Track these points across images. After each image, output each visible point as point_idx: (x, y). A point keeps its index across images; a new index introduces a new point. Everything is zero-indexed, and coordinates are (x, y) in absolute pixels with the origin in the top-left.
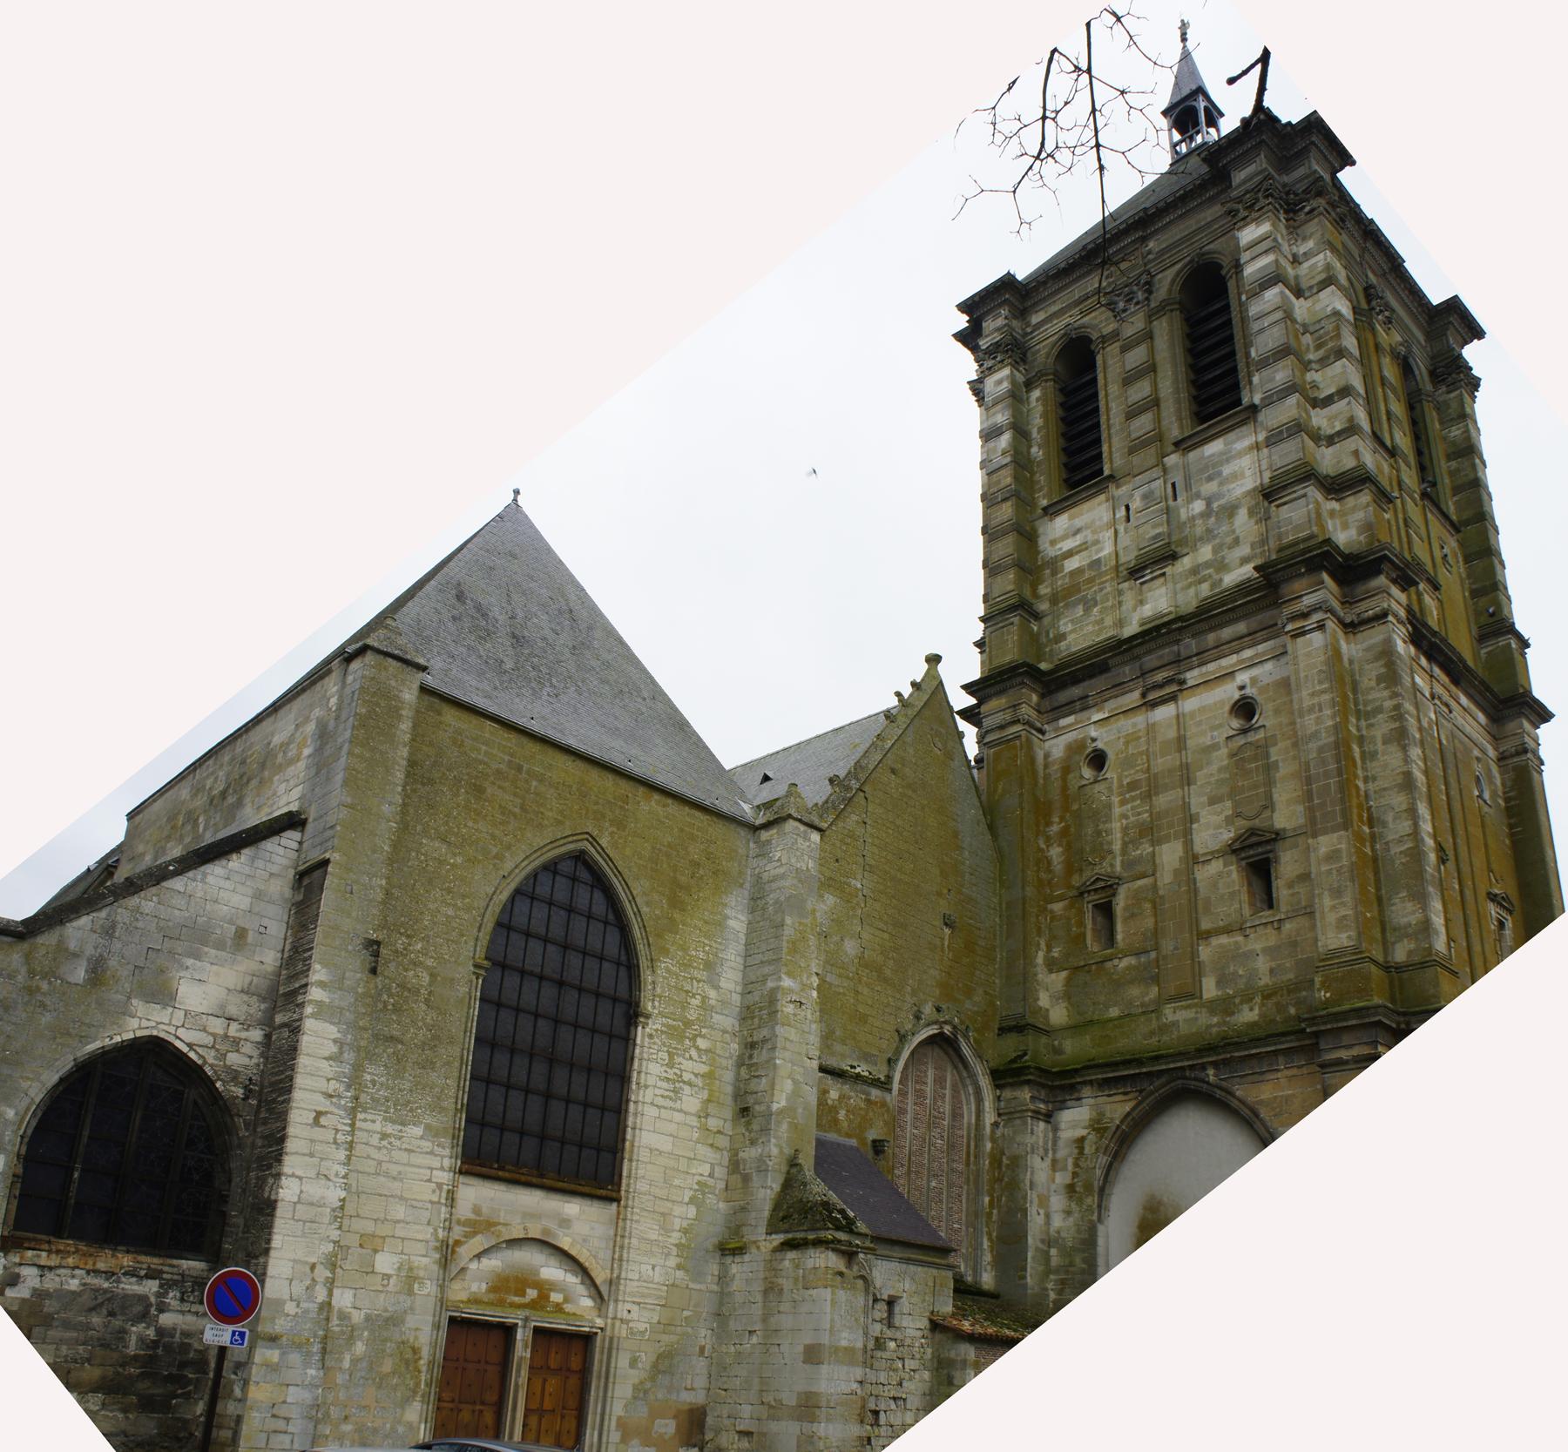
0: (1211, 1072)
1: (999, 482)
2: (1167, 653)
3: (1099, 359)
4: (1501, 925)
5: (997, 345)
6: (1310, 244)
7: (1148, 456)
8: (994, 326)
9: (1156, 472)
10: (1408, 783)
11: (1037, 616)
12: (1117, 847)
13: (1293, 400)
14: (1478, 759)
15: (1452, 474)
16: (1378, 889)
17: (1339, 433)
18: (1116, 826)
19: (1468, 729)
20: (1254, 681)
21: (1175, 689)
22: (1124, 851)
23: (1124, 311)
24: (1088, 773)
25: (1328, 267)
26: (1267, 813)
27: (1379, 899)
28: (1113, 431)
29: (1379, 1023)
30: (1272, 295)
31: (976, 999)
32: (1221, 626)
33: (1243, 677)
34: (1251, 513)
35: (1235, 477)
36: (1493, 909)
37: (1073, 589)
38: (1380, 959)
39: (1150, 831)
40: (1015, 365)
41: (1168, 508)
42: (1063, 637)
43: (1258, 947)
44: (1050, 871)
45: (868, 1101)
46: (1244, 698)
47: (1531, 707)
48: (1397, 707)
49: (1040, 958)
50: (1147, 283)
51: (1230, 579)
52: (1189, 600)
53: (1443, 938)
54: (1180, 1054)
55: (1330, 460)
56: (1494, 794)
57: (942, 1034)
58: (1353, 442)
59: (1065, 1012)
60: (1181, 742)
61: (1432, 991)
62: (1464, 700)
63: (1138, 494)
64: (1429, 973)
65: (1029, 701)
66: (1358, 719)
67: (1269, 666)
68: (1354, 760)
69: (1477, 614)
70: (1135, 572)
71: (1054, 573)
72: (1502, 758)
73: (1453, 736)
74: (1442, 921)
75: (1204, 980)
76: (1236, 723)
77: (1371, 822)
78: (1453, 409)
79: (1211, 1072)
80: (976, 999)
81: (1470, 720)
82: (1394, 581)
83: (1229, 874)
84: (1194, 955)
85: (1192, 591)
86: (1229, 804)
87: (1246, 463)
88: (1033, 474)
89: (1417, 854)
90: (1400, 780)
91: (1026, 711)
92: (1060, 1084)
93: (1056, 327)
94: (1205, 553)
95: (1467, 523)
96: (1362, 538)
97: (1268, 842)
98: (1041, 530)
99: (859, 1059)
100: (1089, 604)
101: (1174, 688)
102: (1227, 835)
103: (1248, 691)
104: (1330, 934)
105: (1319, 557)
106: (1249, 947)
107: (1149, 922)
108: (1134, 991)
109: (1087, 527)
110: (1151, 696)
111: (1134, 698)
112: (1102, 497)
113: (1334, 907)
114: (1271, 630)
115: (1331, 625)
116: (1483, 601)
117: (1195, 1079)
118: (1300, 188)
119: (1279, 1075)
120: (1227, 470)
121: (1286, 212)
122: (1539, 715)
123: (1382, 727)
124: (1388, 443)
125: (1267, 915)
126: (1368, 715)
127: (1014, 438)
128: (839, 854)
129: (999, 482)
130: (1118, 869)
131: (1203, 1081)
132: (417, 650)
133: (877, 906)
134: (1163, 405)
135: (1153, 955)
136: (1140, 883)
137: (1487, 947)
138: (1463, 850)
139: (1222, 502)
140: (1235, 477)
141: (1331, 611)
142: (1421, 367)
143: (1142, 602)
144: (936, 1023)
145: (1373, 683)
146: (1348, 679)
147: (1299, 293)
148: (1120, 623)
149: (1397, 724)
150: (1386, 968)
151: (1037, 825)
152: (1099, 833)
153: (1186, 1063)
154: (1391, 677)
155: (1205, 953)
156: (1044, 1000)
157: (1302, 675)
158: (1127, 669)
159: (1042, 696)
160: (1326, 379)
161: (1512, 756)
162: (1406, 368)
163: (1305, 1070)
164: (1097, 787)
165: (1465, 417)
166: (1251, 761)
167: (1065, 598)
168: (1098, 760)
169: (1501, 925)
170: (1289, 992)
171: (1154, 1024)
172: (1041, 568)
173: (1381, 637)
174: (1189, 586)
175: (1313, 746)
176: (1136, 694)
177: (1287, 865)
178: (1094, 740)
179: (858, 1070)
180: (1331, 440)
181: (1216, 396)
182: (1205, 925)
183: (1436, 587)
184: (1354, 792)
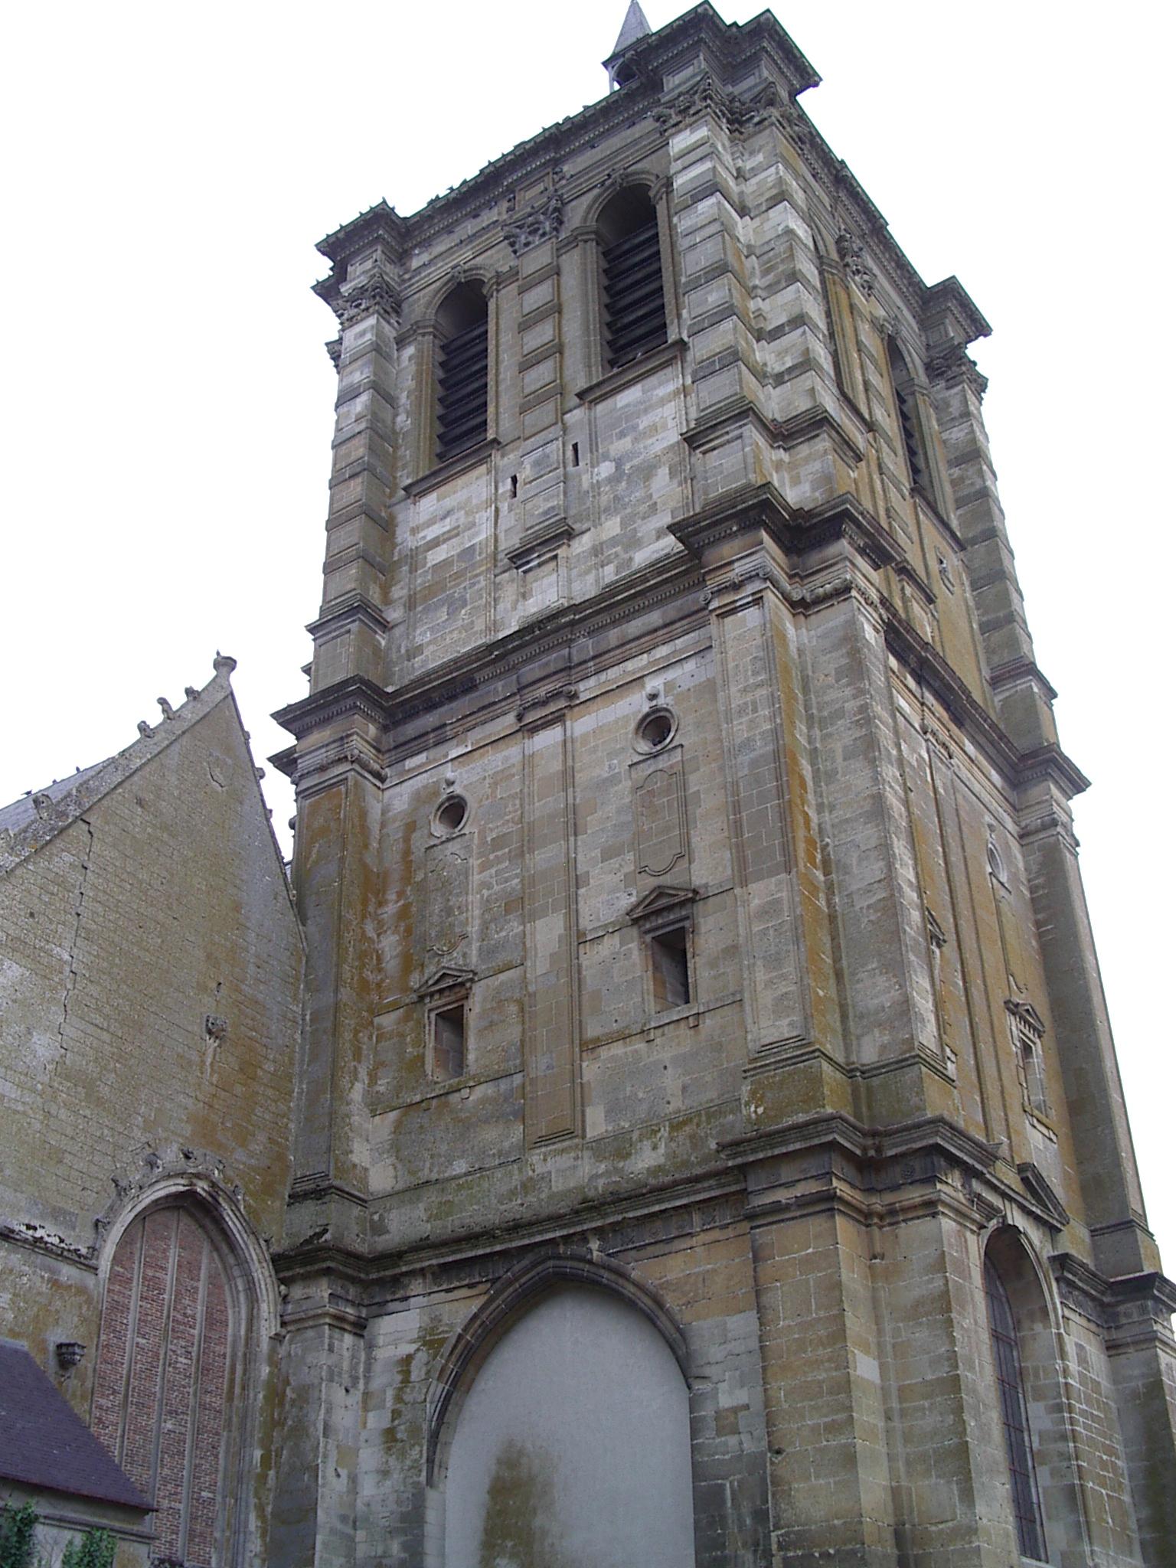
0: (594, 1245)
1: (349, 455)
2: (554, 659)
3: (492, 306)
4: (1027, 1050)
5: (363, 290)
6: (760, 157)
7: (545, 413)
8: (359, 274)
9: (556, 431)
10: (878, 810)
11: (385, 626)
12: (474, 929)
13: (728, 325)
14: (990, 826)
15: (954, 483)
16: (837, 960)
17: (790, 370)
18: (474, 898)
19: (977, 788)
20: (669, 686)
21: (562, 705)
22: (484, 935)
23: (527, 244)
24: (439, 830)
25: (780, 181)
26: (683, 864)
27: (839, 975)
28: (502, 387)
29: (833, 1145)
30: (707, 207)
31: (253, 1147)
32: (627, 617)
33: (654, 684)
34: (672, 474)
35: (654, 429)
36: (1013, 1022)
37: (434, 589)
38: (841, 1060)
39: (519, 904)
40: (385, 314)
41: (565, 475)
42: (419, 649)
43: (666, 1056)
44: (380, 970)
45: (55, 1283)
46: (655, 710)
47: (1060, 769)
48: (864, 708)
49: (357, 1093)
50: (556, 210)
51: (642, 558)
52: (586, 588)
53: (931, 1027)
54: (550, 1218)
55: (775, 403)
56: (1014, 877)
57: (190, 1195)
58: (810, 379)
59: (391, 1172)
60: (568, 776)
61: (915, 1100)
62: (970, 748)
63: (528, 461)
64: (910, 1074)
65: (363, 733)
66: (810, 727)
67: (690, 666)
68: (802, 778)
69: (990, 651)
70: (519, 558)
71: (413, 570)
72: (1023, 836)
73: (955, 791)
74: (930, 1005)
75: (588, 1111)
76: (644, 747)
77: (826, 867)
78: (955, 408)
79: (594, 1245)
80: (253, 1147)
81: (979, 780)
82: (862, 551)
83: (627, 955)
84: (575, 1073)
85: (591, 578)
86: (630, 856)
87: (670, 410)
88: (396, 448)
89: (891, 907)
90: (867, 806)
91: (358, 745)
92: (374, 1278)
93: (440, 271)
94: (612, 527)
95: (974, 541)
96: (817, 494)
97: (682, 904)
98: (400, 517)
99: (42, 1216)
100: (454, 606)
101: (562, 703)
102: (626, 901)
103: (661, 702)
104: (764, 1023)
105: (756, 510)
106: (655, 1057)
107: (514, 1033)
108: (490, 1134)
109: (460, 508)
110: (529, 718)
111: (508, 721)
112: (483, 468)
113: (770, 983)
114: (696, 618)
115: (771, 598)
116: (996, 637)
117: (572, 1258)
118: (747, 97)
119: (694, 1241)
120: (644, 423)
121: (729, 121)
122: (1071, 780)
123: (844, 735)
124: (867, 416)
125: (683, 1011)
126: (823, 723)
127: (373, 400)
128: (38, 907)
129: (349, 455)
130: (474, 959)
131: (582, 1259)
132: (29, 1227)
133: (93, 990)
134: (567, 353)
135: (518, 1079)
136: (502, 977)
137: (1005, 1074)
138: (966, 926)
139: (635, 462)
140: (654, 429)
141: (775, 584)
142: (915, 360)
143: (524, 596)
144: (181, 1175)
145: (831, 680)
146: (795, 673)
147: (743, 211)
148: (495, 626)
149: (864, 731)
150: (849, 1072)
151: (365, 902)
152: (449, 911)
153: (558, 1234)
154: (855, 668)
155: (591, 1070)
156: (360, 1154)
157: (731, 665)
158: (500, 685)
159: (385, 729)
160: (775, 309)
161: (1037, 831)
162: (894, 352)
163: (730, 1232)
164: (451, 847)
165: (967, 416)
166: (664, 800)
167: (425, 599)
168: (454, 811)
169: (1027, 1050)
170: (709, 1117)
171: (516, 1179)
172: (398, 564)
173: (842, 618)
174: (587, 572)
175: (744, 759)
176: (510, 719)
177: (709, 936)
178: (450, 783)
179: (39, 1233)
180: (779, 379)
181: (635, 327)
182: (592, 1031)
183: (930, 600)
184: (800, 819)
